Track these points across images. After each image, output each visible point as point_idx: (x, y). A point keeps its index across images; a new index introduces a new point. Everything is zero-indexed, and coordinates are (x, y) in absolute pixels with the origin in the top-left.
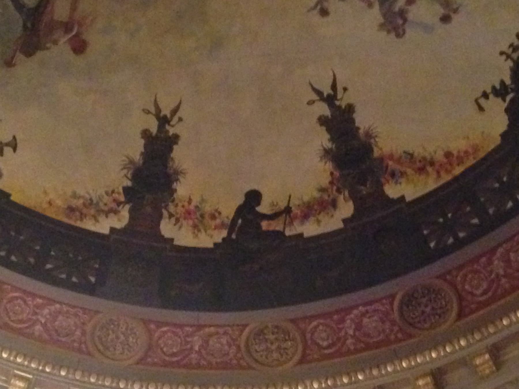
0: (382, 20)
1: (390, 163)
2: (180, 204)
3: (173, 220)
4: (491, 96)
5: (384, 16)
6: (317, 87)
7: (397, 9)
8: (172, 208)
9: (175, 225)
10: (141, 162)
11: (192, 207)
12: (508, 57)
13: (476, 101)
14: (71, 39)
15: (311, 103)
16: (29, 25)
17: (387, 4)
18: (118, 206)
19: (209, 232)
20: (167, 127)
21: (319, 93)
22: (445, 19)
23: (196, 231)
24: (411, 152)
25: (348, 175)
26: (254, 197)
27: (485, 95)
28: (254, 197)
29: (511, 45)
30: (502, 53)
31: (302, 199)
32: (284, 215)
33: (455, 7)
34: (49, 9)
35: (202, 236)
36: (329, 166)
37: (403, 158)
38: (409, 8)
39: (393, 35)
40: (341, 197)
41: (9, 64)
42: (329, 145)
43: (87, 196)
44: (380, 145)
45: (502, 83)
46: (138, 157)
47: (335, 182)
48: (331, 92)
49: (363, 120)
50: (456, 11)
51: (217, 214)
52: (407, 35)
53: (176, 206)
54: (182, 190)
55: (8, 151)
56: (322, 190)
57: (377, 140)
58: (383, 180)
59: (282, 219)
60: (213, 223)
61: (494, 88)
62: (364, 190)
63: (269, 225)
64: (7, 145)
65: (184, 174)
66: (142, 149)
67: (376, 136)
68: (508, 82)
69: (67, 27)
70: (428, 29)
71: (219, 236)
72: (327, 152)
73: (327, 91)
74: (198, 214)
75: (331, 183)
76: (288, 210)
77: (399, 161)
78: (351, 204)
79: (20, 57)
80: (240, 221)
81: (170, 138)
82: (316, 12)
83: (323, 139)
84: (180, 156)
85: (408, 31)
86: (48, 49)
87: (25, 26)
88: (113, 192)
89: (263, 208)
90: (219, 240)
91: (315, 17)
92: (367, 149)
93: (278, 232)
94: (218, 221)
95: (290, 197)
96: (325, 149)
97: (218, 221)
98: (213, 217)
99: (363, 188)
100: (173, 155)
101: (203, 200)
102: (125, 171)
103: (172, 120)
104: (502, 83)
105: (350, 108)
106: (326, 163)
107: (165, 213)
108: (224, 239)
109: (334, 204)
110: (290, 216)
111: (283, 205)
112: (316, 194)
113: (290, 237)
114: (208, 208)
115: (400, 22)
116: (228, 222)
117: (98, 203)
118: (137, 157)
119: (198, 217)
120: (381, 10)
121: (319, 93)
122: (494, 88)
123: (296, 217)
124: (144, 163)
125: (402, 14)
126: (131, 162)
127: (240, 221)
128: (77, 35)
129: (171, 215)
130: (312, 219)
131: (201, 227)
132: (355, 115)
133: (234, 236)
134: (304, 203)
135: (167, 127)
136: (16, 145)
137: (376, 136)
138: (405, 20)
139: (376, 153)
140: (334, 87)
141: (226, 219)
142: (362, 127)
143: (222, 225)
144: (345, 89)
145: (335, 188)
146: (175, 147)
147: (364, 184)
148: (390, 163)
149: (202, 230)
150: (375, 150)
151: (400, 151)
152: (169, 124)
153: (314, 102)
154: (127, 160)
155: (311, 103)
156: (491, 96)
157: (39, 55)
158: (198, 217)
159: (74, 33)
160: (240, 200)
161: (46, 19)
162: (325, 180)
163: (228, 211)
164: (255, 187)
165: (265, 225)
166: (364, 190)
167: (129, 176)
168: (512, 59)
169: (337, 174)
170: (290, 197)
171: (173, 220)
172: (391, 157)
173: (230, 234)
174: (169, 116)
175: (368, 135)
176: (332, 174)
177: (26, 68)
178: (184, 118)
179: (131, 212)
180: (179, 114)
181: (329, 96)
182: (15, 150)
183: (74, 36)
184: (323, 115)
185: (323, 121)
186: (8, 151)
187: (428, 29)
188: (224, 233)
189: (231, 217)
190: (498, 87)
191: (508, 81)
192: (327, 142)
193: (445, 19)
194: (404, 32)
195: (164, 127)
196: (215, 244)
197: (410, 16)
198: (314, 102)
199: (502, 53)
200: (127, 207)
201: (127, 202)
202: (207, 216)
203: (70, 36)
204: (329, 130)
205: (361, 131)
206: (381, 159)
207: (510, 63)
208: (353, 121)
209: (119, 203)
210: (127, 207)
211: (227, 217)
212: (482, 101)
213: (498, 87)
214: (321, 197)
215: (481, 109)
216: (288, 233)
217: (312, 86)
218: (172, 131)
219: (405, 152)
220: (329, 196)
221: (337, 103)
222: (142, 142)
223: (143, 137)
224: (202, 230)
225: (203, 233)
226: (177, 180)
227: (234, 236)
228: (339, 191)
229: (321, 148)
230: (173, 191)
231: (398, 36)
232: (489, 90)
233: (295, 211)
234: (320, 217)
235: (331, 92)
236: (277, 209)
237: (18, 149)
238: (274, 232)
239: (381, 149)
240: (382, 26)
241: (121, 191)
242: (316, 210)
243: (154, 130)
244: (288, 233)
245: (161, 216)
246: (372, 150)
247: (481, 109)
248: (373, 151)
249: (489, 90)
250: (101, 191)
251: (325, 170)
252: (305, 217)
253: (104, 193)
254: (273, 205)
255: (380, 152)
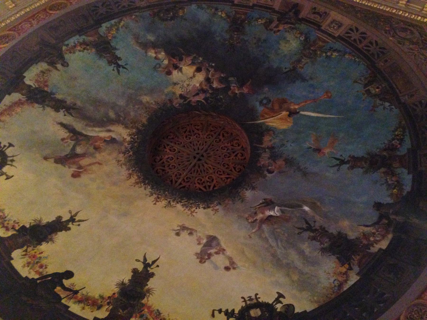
0: (199, 252)
1: (146, 310)
2: (35, 251)
3: (24, 253)
4: (223, 314)
5: (201, 251)
6: (147, 257)
7: (209, 252)
8: (29, 249)
9: (22, 255)
10: (44, 224)
11: (39, 256)
12: (245, 301)
13: (214, 311)
14: (76, 171)
15: (138, 260)
16: (68, 156)
17: (207, 248)
18: (12, 229)
19: (31, 270)
20: (70, 223)
21: (145, 259)
22: (227, 269)
23: (26, 265)
24: (161, 312)
25: (121, 300)
26: (69, 275)
27: (220, 311)
28: (69, 275)
29: (250, 297)
30: (243, 298)
31: (88, 293)
32: (72, 293)
33: (235, 266)
34: (81, 158)
35: (27, 269)
36: (117, 290)
37: (154, 312)
38: (215, 255)
39: (198, 260)
40: (107, 307)
41: (46, 158)
42: (126, 281)
43: (6, 215)
44: (150, 299)
45: (233, 310)
46: (45, 222)
47: (112, 298)
48: (151, 263)
49: (151, 283)
50: (234, 268)
51: (44, 267)
52: (204, 265)
53: (33, 250)
54: (44, 247)
55: (4, 177)
56: (102, 297)
57: (151, 296)
58: (134, 315)
59: (68, 293)
60: (37, 269)
61: (227, 310)
62: (121, 312)
63: (60, 291)
64: (7, 175)
65: (53, 243)
66: (50, 221)
67: (151, 294)
68: (236, 312)
69: (80, 167)
70: (216, 267)
71: (33, 275)
72: (123, 283)
73: (149, 261)
74: (37, 260)
75: (109, 297)
76: (76, 292)
77: (151, 312)
78: (107, 314)
79: (52, 160)
80: (50, 278)
81: (66, 227)
82: (174, 232)
83: (127, 277)
84: (61, 237)
85: (206, 263)
86: (65, 167)
87: (67, 155)
88: (18, 223)
89: (66, 283)
90: (30, 277)
91: (173, 234)
92: (142, 296)
93: (60, 297)
94: (41, 270)
95: (85, 288)
96: (123, 282)
97: (41, 270)
98: (41, 267)
99: (121, 311)
100: (59, 233)
101: (46, 258)
102: (33, 222)
103: (76, 222)
104: (233, 310)
105: (152, 275)
106: (117, 287)
107: (25, 248)
108: (33, 279)
109: (99, 307)
110: (73, 295)
111: (77, 288)
112: (97, 296)
113: (63, 304)
114: (44, 262)
115: (206, 257)
116: (44, 273)
117: (6, 221)
118: (44, 222)
119: (35, 261)
120: (201, 249)
121: (145, 259)
122: (227, 310)
123: (75, 298)
124: (44, 226)
125: (210, 255)
126: (40, 221)
127: (50, 278)
128: (80, 172)
129: (26, 251)
130: (82, 305)
131: (30, 266)
132: (151, 279)
133: (38, 281)
134: (87, 295)
135: (70, 223)
136: (9, 179)
137: (151, 294)
138: (209, 258)
139: (144, 301)
140: (154, 262)
141: (45, 272)
142: (149, 286)
143: (40, 273)
144: (158, 266)
145: (109, 301)
146: (63, 232)
147: (123, 310)
148: (146, 310)
149: (30, 267)
150: (146, 299)
151: (156, 308)
152: (72, 223)
153: (139, 261)
154: (39, 218)
155: (138, 260)
156: (223, 314)
157: (59, 166)
158: (35, 261)
159: (80, 171)
160: (61, 270)
161: (77, 160)
162: (108, 294)
163: (51, 270)
164: (74, 272)
165: (58, 289)
166: (121, 312)
167: (32, 224)
168: (246, 303)
169: (116, 295)
170: (85, 288)
171: (24, 253)
172: (149, 308)
173: (38, 279)
174: (76, 220)
175: (148, 291)
176: (114, 294)
177: (50, 165)
178: (81, 226)
179: (13, 235)
180: (80, 223)
181: (149, 263)
182: (7, 179)
183: (79, 172)
184: (137, 269)
185: (135, 271)
186: (4, 177)
187: (216, 267)
188: (36, 277)
189: (48, 274)
190: (230, 311)
191: (236, 312)
192: (127, 280)
193: (227, 269)
194: (205, 262)
195: (70, 222)
196: (26, 277)
197: (212, 258)
198: (139, 261)
199: (243, 298)
200: (15, 232)
201: (17, 231)
202: (39, 264)
203: (77, 170)
204: (133, 276)
205: (147, 287)
206: (143, 305)
207: (244, 304)
208: (148, 280)
209: (13, 228)
210: (15, 232)
211: (47, 272)
212: (216, 313)
213: (230, 311)
214: (98, 300)
215: (213, 315)
216: (63, 301)
217: (145, 254)
218: (70, 225)
219: (158, 310)
220: (102, 302)
221: (149, 269)
222: (54, 219)
223: (56, 218)
224: (30, 267)
225: (28, 268)
226: (48, 242)
227: (38, 281)
228: (108, 304)
229: (122, 281)
230: (40, 243)
231: (200, 262)
232: (224, 310)
233: (79, 295)
234: (87, 307)
235: (151, 263)
236: (72, 288)
237: (8, 180)
238: (58, 295)
239: (148, 301)
240: (197, 254)
241: (22, 225)
242: (89, 303)
243: (64, 220)
244: (63, 301)
245: (22, 247)
246: (144, 298)
247: (213, 315)
248: (144, 299)
249: (224, 310)
250: (15, 219)
251: (112, 290)
252: (80, 301)
253: (13, 220)
254: (73, 285)
255: (146, 302)
